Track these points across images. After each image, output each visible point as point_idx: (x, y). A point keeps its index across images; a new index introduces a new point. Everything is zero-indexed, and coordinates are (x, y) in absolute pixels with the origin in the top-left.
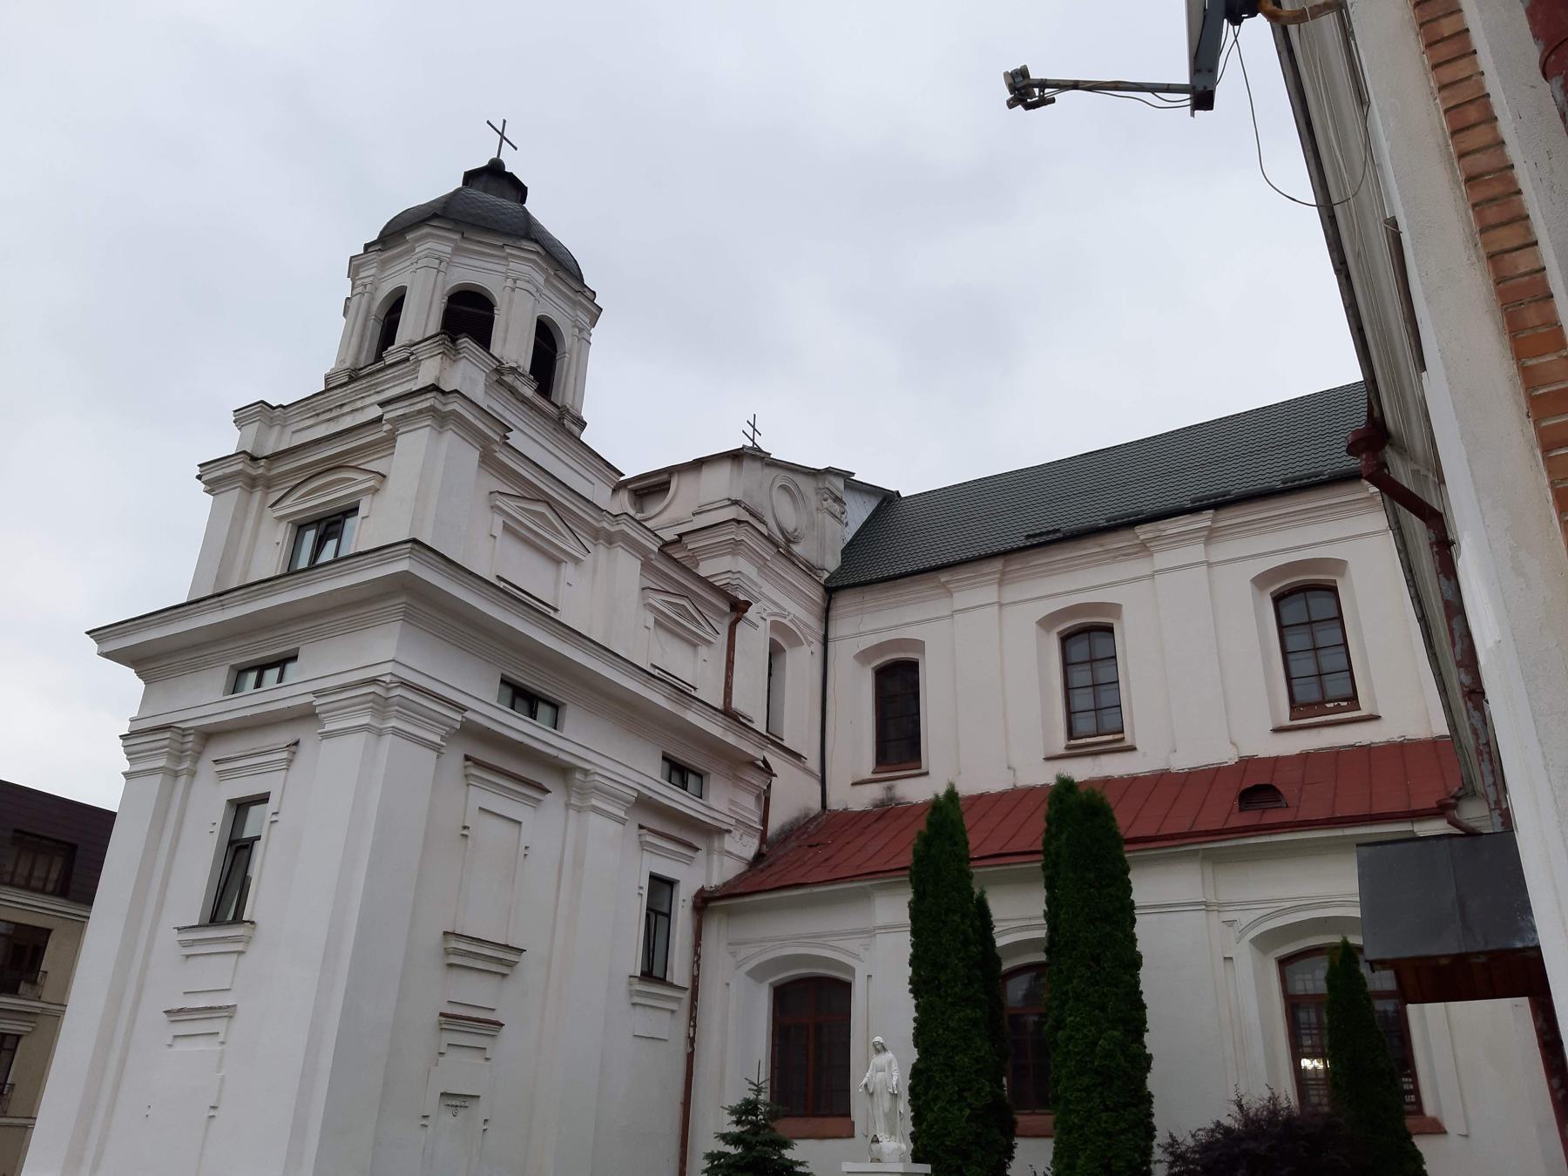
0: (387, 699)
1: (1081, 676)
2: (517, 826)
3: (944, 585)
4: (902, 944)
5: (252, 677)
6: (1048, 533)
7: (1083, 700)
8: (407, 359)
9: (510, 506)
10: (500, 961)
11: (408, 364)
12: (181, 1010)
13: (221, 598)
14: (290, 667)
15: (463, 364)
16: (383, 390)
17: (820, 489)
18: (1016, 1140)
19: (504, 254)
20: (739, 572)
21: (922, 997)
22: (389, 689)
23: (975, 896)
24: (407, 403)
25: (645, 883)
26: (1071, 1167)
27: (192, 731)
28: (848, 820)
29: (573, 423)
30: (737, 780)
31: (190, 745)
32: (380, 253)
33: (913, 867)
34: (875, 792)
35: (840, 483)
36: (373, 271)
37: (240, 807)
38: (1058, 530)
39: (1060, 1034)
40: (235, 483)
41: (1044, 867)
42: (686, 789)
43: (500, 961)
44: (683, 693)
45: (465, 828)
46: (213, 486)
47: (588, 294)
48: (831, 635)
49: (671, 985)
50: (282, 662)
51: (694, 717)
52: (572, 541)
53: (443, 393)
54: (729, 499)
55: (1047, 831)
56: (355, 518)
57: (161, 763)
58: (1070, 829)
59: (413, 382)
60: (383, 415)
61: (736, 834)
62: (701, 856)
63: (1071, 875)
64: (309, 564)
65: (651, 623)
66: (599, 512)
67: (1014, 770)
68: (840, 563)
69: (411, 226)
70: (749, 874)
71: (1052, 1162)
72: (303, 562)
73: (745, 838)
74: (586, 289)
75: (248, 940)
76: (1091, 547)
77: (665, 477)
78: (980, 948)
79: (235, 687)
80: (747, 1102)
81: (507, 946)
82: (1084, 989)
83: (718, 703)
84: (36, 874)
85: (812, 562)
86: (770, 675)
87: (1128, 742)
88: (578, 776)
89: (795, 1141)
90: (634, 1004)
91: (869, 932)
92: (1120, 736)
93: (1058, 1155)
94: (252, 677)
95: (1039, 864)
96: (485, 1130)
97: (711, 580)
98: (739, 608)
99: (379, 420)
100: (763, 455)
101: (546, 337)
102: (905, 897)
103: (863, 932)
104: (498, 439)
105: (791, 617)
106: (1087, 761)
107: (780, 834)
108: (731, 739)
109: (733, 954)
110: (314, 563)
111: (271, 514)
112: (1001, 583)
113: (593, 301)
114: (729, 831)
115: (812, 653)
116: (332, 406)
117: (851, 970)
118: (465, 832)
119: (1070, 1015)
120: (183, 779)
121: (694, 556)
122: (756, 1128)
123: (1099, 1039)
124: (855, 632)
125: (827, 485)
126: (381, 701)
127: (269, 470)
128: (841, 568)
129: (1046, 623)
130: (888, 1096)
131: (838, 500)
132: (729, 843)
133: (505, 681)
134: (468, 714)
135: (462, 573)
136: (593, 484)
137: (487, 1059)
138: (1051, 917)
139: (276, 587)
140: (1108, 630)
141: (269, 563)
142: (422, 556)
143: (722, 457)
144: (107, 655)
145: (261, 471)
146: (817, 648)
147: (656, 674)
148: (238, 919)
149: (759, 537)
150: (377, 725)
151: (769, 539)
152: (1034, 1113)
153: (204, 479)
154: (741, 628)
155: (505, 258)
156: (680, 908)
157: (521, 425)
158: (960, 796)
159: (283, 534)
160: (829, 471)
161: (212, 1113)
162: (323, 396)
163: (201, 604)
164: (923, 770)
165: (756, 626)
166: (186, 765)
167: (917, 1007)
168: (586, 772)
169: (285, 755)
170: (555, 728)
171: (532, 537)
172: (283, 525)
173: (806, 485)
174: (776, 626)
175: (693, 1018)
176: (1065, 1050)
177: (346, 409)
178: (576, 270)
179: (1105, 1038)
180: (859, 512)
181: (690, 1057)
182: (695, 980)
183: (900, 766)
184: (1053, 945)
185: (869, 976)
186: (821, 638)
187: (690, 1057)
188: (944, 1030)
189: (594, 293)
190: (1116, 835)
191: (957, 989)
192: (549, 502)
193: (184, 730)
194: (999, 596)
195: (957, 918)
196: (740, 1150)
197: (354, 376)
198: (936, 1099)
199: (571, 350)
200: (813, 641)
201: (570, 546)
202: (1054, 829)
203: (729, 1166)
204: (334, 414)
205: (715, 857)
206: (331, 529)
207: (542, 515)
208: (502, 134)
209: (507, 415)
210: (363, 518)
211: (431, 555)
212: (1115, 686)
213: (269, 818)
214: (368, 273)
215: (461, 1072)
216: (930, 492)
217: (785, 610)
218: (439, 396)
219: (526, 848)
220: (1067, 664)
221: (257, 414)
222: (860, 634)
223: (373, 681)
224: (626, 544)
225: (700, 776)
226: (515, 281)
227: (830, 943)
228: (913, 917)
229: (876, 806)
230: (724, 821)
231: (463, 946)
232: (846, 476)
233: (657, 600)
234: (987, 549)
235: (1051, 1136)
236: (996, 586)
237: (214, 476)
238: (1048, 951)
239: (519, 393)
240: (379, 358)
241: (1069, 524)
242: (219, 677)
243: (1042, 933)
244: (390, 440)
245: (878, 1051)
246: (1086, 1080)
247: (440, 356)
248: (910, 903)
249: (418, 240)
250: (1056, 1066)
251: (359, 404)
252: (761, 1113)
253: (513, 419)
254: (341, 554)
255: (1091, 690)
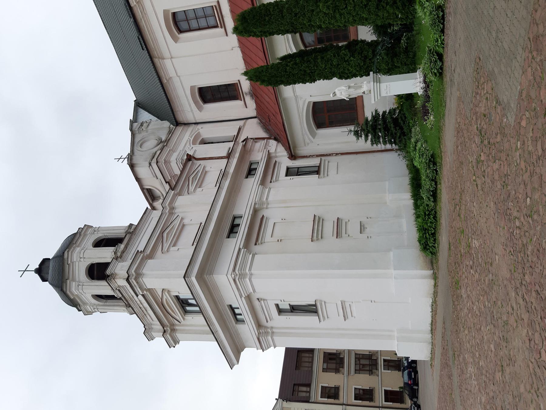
0: (240, 275)
1: (194, 24)
2: (276, 224)
3: (168, 81)
4: (299, 87)
5: (238, 317)
6: (140, 41)
7: (203, 23)
8: (119, 290)
9: (166, 246)
10: (319, 222)
11: (120, 290)
12: (344, 317)
13: (214, 332)
14: (234, 306)
15: (117, 271)
16: (132, 295)
17: (139, 132)
18: (359, 39)
19: (71, 263)
20: (176, 159)
21: (316, 78)
22: (237, 275)
23: (280, 62)
24: (135, 288)
25: (289, 178)
26: (366, 19)
27: (259, 331)
28: (259, 108)
29: (131, 228)
30: (251, 150)
31: (263, 331)
32: (81, 306)
33: (273, 86)
34: (248, 99)
35: (135, 125)
36: (88, 307)
37: (280, 311)
38: (138, 37)
39: (323, 26)
40: (174, 336)
41: (266, 36)
42: (256, 168)
43: (319, 222)
44: (224, 174)
45: (278, 241)
46: (176, 342)
47: (80, 230)
48: (194, 122)
49: (320, 164)
50: (232, 309)
51: (231, 170)
52: (175, 222)
53: (129, 276)
54: (149, 167)
55: (253, 36)
56: (180, 296)
57: (270, 338)
58: (251, 28)
59: (127, 287)
60: (141, 295)
61: (269, 148)
62: (277, 159)
63: (268, 26)
64: (197, 307)
65: (200, 189)
66: (163, 214)
67: (233, 47)
68: (166, 121)
69: (67, 297)
70: (282, 142)
71: (365, 26)
72: (197, 309)
73: (270, 145)
74: (79, 232)
75: (321, 301)
76: (143, 24)
77: (145, 191)
78: (297, 58)
79: (243, 321)
80: (355, 134)
81: (314, 220)
82: (307, 19)
83: (225, 161)
84: (307, 361)
85: (168, 132)
86: (212, 143)
87: (216, 4)
88: (257, 206)
89: (365, 116)
90: (327, 175)
91: (296, 98)
92: (214, 8)
93: (363, 24)
94: (238, 317)
95: (266, 38)
96: (370, 218)
97: (181, 169)
98: (190, 158)
99: (143, 295)
100: (130, 156)
101: (100, 243)
102: (282, 87)
103: (296, 100)
104: (142, 255)
105: (190, 138)
106: (225, 19)
107: (267, 132)
108: (237, 155)
109: (308, 144)
110: (197, 305)
111: (183, 322)
112: (163, 59)
113: (83, 228)
114: (269, 151)
115: (202, 128)
116: (141, 311)
117: (309, 102)
118: (280, 240)
119: (316, 23)
120: (274, 330)
121: (174, 176)
122: (363, 130)
123: (323, 12)
124: (191, 113)
125: (137, 129)
126: (240, 276)
127: (167, 326)
128: (168, 120)
129: (176, 40)
130: (349, 90)
131: (142, 125)
132: (272, 150)
133: (228, 237)
134: (241, 247)
135: (193, 259)
136: (153, 217)
137: (349, 221)
138: (283, 32)
139: (207, 316)
140: (174, 14)
141: (199, 319)
142: (189, 273)
143: (133, 171)
144: (238, 362)
145: (168, 328)
146: (199, 126)
147: (219, 184)
148: (315, 305)
149: (162, 153)
150: (249, 275)
151: (162, 150)
152: (350, 32)
153: (174, 345)
154: (197, 156)
155: (73, 263)
156: (295, 165)
157: (136, 246)
158: (245, 70)
159: (189, 317)
160: (131, 129)
161: (373, 302)
162: (138, 315)
163: (217, 338)
164: (238, 82)
165: (195, 151)
166: (269, 330)
167: (319, 80)
168: (255, 204)
169: (262, 302)
170: (242, 217)
171: (176, 236)
172: (186, 317)
173: (138, 138)
174: (194, 143)
175: (330, 155)
176: (328, 24)
177: (141, 306)
178: (72, 236)
179: (323, 10)
180: (145, 116)
181: (342, 154)
182: (318, 156)
183: (238, 91)
184: (293, 31)
185: (311, 96)
186: (196, 125)
187: (342, 154)
188: (326, 69)
189: (79, 228)
190: (251, 10)
191: (312, 66)
192: (162, 233)
193: (258, 334)
194: (169, 59)
195: (288, 68)
196: (370, 135)
197: (128, 306)
198: (348, 70)
199: (103, 233)
200: (197, 128)
201: (177, 222)
202: (253, 34)
203: (375, 138)
204: (144, 309)
205: (278, 155)
206: (185, 302)
207: (168, 234)
208: (24, 271)
209: (132, 252)
210: (179, 293)
211: (188, 270)
212: (195, 10)
213: (283, 302)
214: (89, 308)
215: (353, 228)
216: (132, 88)
217: (188, 140)
218: (130, 278)
219: (282, 220)
220: (190, 30)
221: (148, 334)
222: (192, 111)
223: (234, 280)
224: (173, 203)
225: (251, 164)
226: (81, 258)
227: (301, 111)
228: (290, 84)
229: (253, 98)
230: (265, 154)
231: (315, 235)
232: (132, 122)
233: (192, 188)
234: (149, 61)
235: (357, 28)
236: (164, 60)
237: (173, 342)
238: (295, 33)
239: (124, 249)
240: (120, 299)
241: (135, 34)
242: (240, 327)
243: (290, 36)
244: (150, 290)
245: (335, 95)
246: (338, 16)
247: (115, 280)
248: (285, 86)
249: (73, 294)
250: (334, 27)
251: (139, 302)
252: (358, 129)
253: (134, 250)
254: (192, 298)
255: (198, 19)
